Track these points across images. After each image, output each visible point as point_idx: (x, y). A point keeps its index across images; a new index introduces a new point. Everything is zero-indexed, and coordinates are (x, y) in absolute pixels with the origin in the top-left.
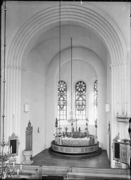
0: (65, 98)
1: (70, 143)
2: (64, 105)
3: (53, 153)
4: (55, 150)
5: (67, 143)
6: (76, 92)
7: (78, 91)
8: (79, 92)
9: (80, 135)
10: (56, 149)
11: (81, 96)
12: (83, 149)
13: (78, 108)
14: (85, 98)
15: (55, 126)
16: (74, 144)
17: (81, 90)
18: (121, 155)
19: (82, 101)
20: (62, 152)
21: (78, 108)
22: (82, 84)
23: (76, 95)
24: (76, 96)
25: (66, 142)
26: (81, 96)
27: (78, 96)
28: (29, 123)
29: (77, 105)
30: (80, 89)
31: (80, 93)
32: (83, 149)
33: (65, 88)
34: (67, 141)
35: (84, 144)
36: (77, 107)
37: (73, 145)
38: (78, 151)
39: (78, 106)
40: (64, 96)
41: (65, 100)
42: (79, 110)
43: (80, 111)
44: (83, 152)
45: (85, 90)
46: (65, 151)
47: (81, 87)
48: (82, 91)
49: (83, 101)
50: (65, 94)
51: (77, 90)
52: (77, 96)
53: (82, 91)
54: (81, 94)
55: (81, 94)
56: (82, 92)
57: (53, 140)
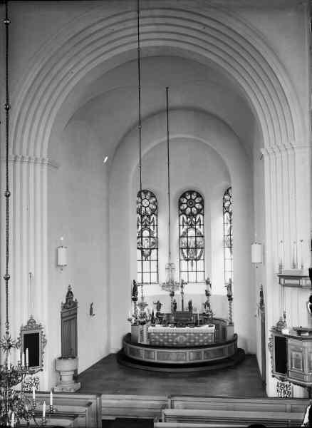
2: (151, 249)
6: (224, 213)
7: (185, 214)
8: (188, 216)
9: (191, 320)
10: (134, 355)
11: (191, 225)
12: (198, 354)
18: (292, 366)
22: (193, 197)
23: (181, 224)
24: (181, 227)
27: (186, 227)
29: (182, 249)
31: (189, 219)
32: (200, 352)
36: (183, 253)
39: (185, 251)
40: (152, 228)
41: (155, 235)
42: (188, 260)
47: (191, 203)
48: (195, 213)
50: (199, 220)
51: (183, 212)
53: (195, 213)
55: (191, 220)
56: (194, 216)
57: (127, 333)
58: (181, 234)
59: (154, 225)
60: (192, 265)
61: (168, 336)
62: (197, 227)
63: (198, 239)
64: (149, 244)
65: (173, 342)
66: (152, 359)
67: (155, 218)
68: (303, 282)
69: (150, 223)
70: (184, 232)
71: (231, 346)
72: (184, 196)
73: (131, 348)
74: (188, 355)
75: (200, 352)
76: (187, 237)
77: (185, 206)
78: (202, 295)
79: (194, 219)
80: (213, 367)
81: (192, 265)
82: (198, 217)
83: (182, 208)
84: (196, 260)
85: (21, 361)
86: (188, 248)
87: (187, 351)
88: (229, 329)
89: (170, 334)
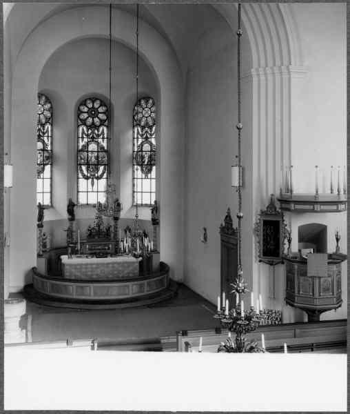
0: (49, 143)
1: (86, 272)
2: (44, 165)
3: (48, 303)
4: (53, 294)
5: (79, 274)
6: (134, 127)
7: (85, 124)
8: (89, 127)
9: (109, 249)
10: (58, 292)
11: (93, 138)
12: (141, 286)
13: (85, 173)
14: (105, 144)
15: (36, 225)
16: (97, 275)
17: (93, 123)
18: (299, 291)
19: (96, 154)
20: (83, 297)
21: (85, 173)
22: (96, 105)
23: (136, 136)
24: (80, 140)
25: (73, 270)
26: (93, 138)
27: (86, 140)
28: (227, 217)
29: (80, 165)
30: (90, 120)
31: (90, 131)
32: (144, 284)
33: (49, 115)
34: (78, 267)
35: (126, 272)
36: (82, 170)
37: (94, 277)
38: (131, 292)
39: (84, 168)
40: (45, 139)
41: (49, 148)
42: (87, 178)
43: (90, 180)
44: (143, 292)
45: (50, 121)
46: (92, 293)
47: (93, 113)
48: (98, 124)
49: (100, 154)
50: (47, 131)
51: (84, 122)
52: (83, 138)
53: (98, 124)
54: (93, 132)
55: (93, 132)
56: (97, 128)
57: (32, 267)
58: (80, 148)
59: (48, 137)
60: (93, 185)
61: (86, 268)
62: (100, 140)
63: (101, 154)
64: (42, 158)
65: (92, 275)
66: (87, 295)
67: (50, 127)
68: (342, 207)
69: (44, 133)
70: (83, 146)
71: (163, 278)
72: (84, 103)
73: (53, 285)
74: (130, 288)
75: (144, 284)
76: (88, 151)
77: (86, 109)
78: (149, 221)
79: (96, 131)
80: (82, 306)
81: (93, 185)
82: (101, 129)
83: (82, 117)
84: (98, 178)
85: (111, 295)
86: (88, 164)
87: (129, 284)
88: (155, 256)
89: (89, 266)
